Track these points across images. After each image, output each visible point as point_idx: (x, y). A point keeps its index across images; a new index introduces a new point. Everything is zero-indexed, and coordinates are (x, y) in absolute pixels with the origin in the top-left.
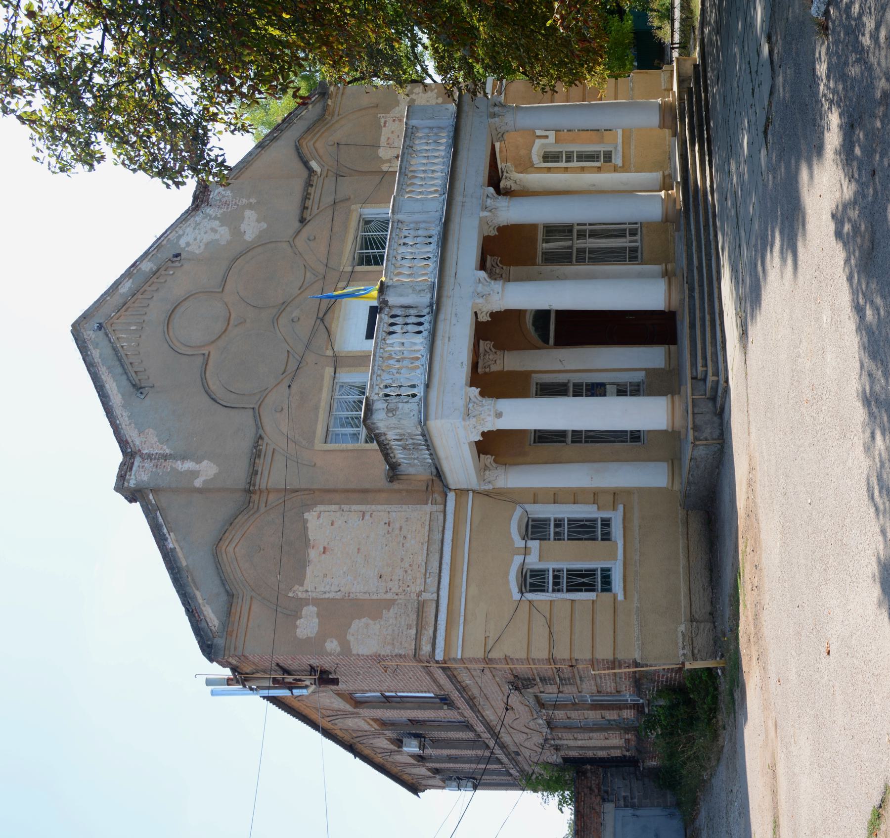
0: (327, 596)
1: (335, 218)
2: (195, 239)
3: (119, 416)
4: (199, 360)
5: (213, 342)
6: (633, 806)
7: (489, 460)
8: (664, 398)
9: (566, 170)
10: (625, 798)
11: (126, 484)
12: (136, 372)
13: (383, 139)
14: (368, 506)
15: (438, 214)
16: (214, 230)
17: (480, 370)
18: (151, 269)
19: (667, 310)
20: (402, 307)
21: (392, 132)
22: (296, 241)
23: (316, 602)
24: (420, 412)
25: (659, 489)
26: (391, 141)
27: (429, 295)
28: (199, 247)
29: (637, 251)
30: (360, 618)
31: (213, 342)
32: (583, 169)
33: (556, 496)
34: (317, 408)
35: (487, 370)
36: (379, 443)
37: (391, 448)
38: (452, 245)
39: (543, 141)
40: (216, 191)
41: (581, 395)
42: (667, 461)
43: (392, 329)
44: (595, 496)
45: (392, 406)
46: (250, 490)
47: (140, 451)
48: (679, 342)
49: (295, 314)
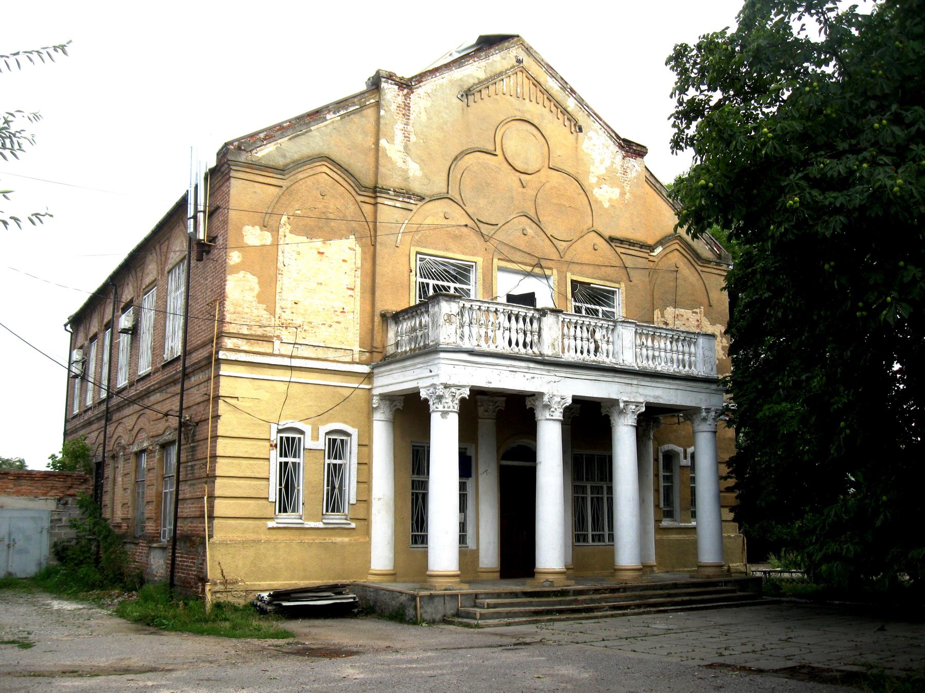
0: (280, 253)
4: (490, 148)
6: (52, 528)
9: (656, 475)
10: (60, 520)
11: (383, 80)
12: (480, 91)
13: (682, 311)
16: (602, 162)
17: (479, 397)
20: (540, 328)
23: (275, 244)
25: (368, 562)
26: (680, 318)
27: (550, 354)
29: (584, 541)
30: (259, 283)
32: (657, 491)
33: (365, 464)
34: (447, 250)
35: (479, 404)
36: (417, 306)
37: (413, 316)
38: (594, 375)
39: (682, 455)
43: (521, 320)
44: (365, 501)
45: (453, 319)
46: (376, 191)
48: (503, 581)
49: (530, 231)
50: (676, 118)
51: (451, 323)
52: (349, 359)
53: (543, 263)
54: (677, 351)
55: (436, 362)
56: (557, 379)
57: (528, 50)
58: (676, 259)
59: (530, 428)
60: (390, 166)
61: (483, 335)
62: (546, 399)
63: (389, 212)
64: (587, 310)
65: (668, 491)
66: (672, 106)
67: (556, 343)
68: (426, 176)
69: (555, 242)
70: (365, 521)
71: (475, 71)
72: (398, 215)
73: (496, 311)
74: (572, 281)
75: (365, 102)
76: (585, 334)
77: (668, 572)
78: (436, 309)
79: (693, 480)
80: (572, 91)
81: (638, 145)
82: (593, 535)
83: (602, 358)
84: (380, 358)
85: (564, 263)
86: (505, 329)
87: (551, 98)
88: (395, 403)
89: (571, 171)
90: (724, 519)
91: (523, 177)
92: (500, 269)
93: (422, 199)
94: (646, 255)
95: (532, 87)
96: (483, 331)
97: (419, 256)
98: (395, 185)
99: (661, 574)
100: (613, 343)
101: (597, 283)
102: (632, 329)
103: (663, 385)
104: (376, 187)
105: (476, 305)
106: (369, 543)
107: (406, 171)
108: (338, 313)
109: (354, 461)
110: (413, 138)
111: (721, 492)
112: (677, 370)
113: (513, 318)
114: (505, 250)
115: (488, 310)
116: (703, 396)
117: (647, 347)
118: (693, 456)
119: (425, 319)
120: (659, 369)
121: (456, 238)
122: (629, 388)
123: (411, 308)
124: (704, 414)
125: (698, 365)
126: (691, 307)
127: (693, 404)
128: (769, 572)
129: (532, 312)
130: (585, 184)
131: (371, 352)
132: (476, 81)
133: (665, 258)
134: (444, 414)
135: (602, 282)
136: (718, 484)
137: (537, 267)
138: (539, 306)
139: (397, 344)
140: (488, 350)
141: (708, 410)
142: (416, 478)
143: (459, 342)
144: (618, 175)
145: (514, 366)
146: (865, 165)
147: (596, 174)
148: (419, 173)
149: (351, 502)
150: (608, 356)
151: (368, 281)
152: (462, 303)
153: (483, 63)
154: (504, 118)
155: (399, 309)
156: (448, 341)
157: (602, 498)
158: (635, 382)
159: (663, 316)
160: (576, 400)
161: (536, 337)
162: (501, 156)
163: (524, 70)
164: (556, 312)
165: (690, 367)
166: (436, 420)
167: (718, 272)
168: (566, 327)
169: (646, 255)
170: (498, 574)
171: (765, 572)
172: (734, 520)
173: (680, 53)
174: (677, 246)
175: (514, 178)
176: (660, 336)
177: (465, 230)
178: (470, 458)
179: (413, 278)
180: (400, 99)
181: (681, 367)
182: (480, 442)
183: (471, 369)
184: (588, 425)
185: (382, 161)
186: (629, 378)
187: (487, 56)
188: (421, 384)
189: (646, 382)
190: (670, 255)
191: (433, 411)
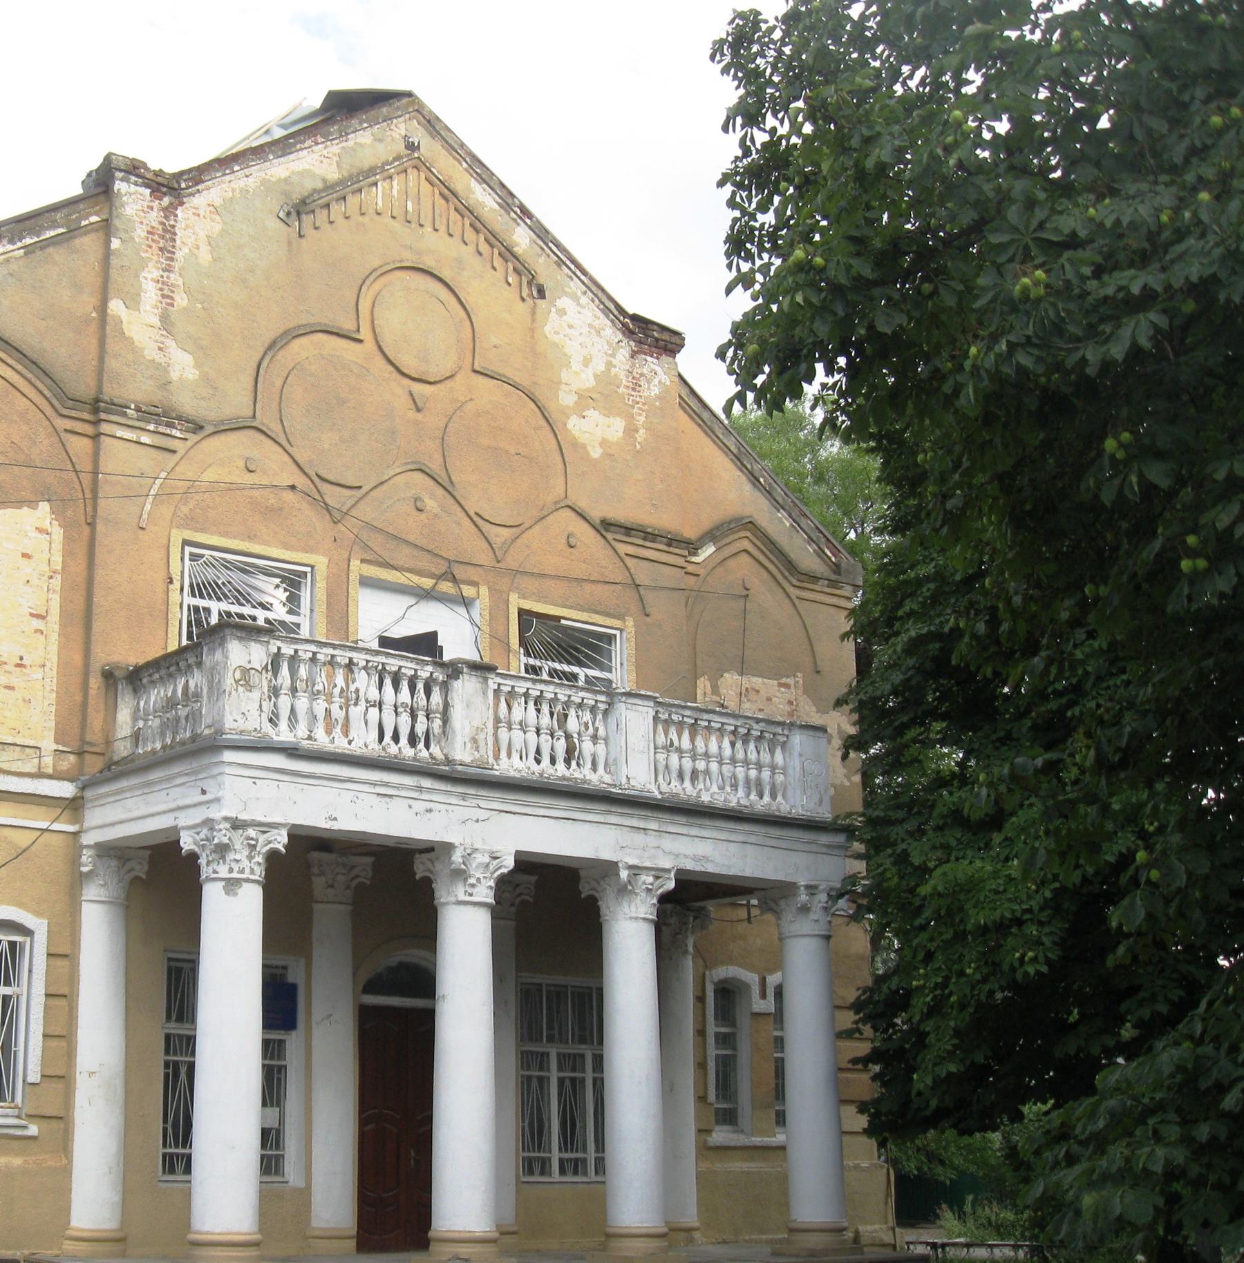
1: (607, 587)
2: (571, 327)
3: (247, 171)
4: (348, 325)
5: (380, 348)
7: (137, 867)
8: (255, 1228)
9: (701, 1033)
11: (119, 175)
13: (757, 681)
14: (57, 627)
15: (624, 781)
16: (586, 362)
17: (315, 855)
18: (517, 245)
19: (431, 1234)
20: (446, 705)
21: (769, 699)
22: (568, 513)
24: (242, 732)
26: (752, 695)
27: (468, 760)
28: (557, 333)
29: (542, 1173)
31: (380, 348)
32: (701, 1065)
33: (63, 996)
34: (250, 538)
35: (315, 870)
36: (182, 651)
37: (170, 675)
38: (562, 807)
39: (756, 990)
40: (657, 369)
41: (265, 1056)
42: (121, 1230)
44: (60, 1076)
45: (255, 678)
46: (97, 409)
47: (182, 204)
49: (430, 504)
50: (735, 184)
51: (249, 687)
52: (30, 767)
53: (459, 571)
54: (746, 762)
55: (216, 771)
56: (482, 814)
57: (432, 124)
58: (744, 569)
59: (424, 925)
60: (130, 357)
61: (321, 714)
62: (457, 857)
63: (126, 452)
64: (553, 673)
65: (726, 1068)
66: (725, 151)
67: (481, 736)
68: (206, 379)
69: (485, 527)
70: (60, 1121)
71: (316, 163)
72: (145, 460)
73: (350, 665)
74: (522, 612)
75: (79, 219)
76: (545, 720)
77: (725, 1242)
78: (218, 655)
79: (780, 1043)
80: (525, 212)
81: (664, 329)
82: (561, 1161)
83: (583, 774)
84: (100, 767)
85: (505, 573)
86: (370, 704)
87: (478, 223)
88: (129, 865)
89: (524, 380)
90: (845, 1129)
91: (418, 388)
92: (366, 582)
93: (198, 427)
94: (681, 562)
95: (440, 201)
96: (320, 706)
97: (188, 549)
98: (140, 397)
99: (710, 1248)
100: (606, 740)
101: (575, 618)
102: (648, 710)
103: (714, 834)
104: (97, 400)
105: (306, 651)
106: (67, 1171)
107: (164, 369)
108: (9, 667)
109: (39, 988)
110: (181, 300)
111: (840, 1069)
112: (744, 802)
113: (388, 682)
114: (376, 541)
115: (332, 662)
116: (799, 859)
117: (679, 750)
118: (779, 992)
119: (196, 680)
120: (706, 798)
121: (271, 513)
122: (639, 838)
123: (167, 657)
124: (803, 897)
125: (790, 793)
126: (775, 674)
127: (780, 876)
128: (943, 1246)
129: (430, 668)
130: (551, 407)
131: (80, 754)
132: (320, 185)
133: (720, 569)
134: (232, 885)
135: (585, 616)
136: (836, 1052)
137: (445, 581)
138: (447, 657)
139: (136, 737)
140: (331, 748)
141: (812, 889)
142: (175, 1028)
143: (267, 728)
144: (621, 390)
145: (387, 785)
146: (1204, 196)
147: (574, 387)
148: (192, 374)
149: (30, 1079)
150: (594, 767)
151: (79, 600)
152: (274, 646)
153: (335, 148)
154: (376, 263)
155: (141, 661)
156: (241, 725)
157: (583, 1080)
158: (653, 825)
159: (715, 690)
160: (527, 864)
161: (437, 723)
162: (370, 344)
163: (421, 165)
164: (481, 669)
165: (773, 796)
166: (213, 896)
167: (834, 600)
168: (503, 704)
169: (681, 562)
170: (352, 1244)
171: (934, 1246)
172: (868, 1132)
173: (745, 32)
174: (746, 544)
175: (400, 391)
176: (708, 728)
177: (289, 496)
178: (293, 988)
179: (175, 597)
180: (155, 217)
181: (753, 797)
182: (315, 954)
183: (290, 788)
184: (550, 914)
185: (112, 346)
186: (640, 817)
187: (343, 134)
188: (185, 819)
189: (677, 825)
190: (731, 563)
191: (209, 879)
